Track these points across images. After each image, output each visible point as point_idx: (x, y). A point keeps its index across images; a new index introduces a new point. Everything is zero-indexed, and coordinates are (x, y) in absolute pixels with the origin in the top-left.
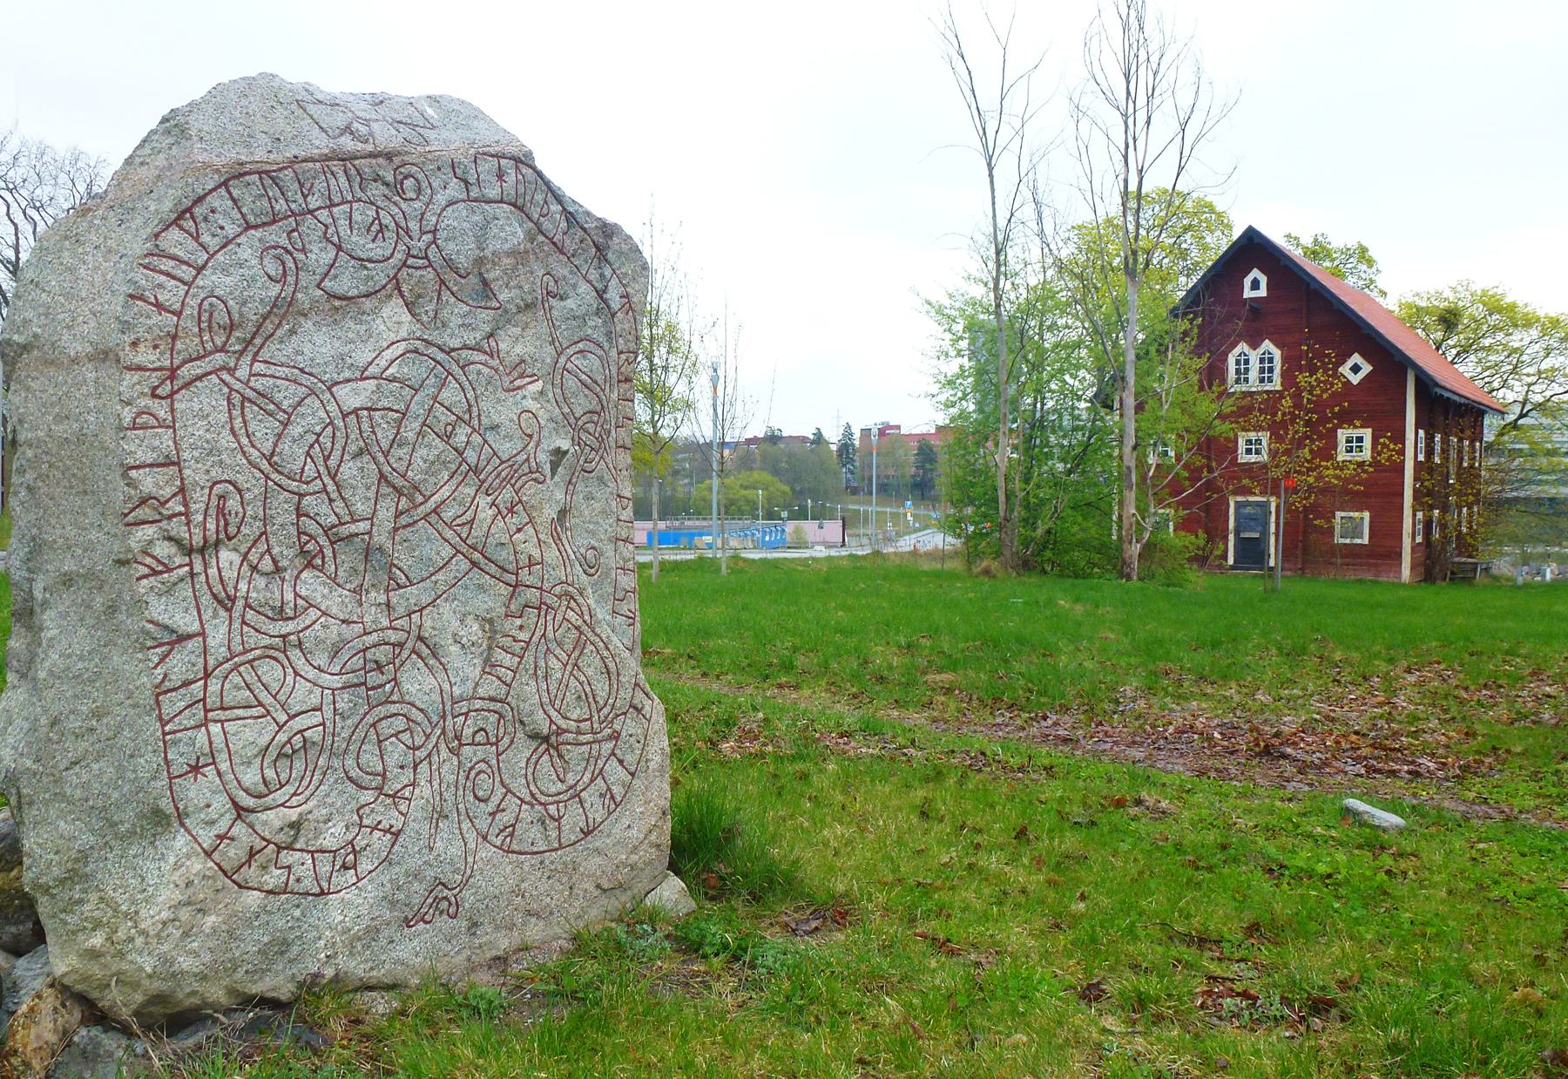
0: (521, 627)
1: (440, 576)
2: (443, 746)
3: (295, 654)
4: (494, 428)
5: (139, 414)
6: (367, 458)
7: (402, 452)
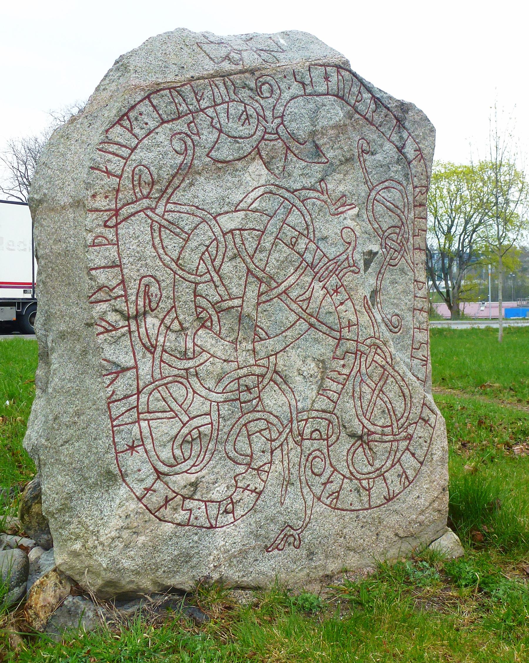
0: (344, 366)
1: (288, 333)
2: (290, 440)
3: (193, 380)
4: (324, 239)
5: (97, 237)
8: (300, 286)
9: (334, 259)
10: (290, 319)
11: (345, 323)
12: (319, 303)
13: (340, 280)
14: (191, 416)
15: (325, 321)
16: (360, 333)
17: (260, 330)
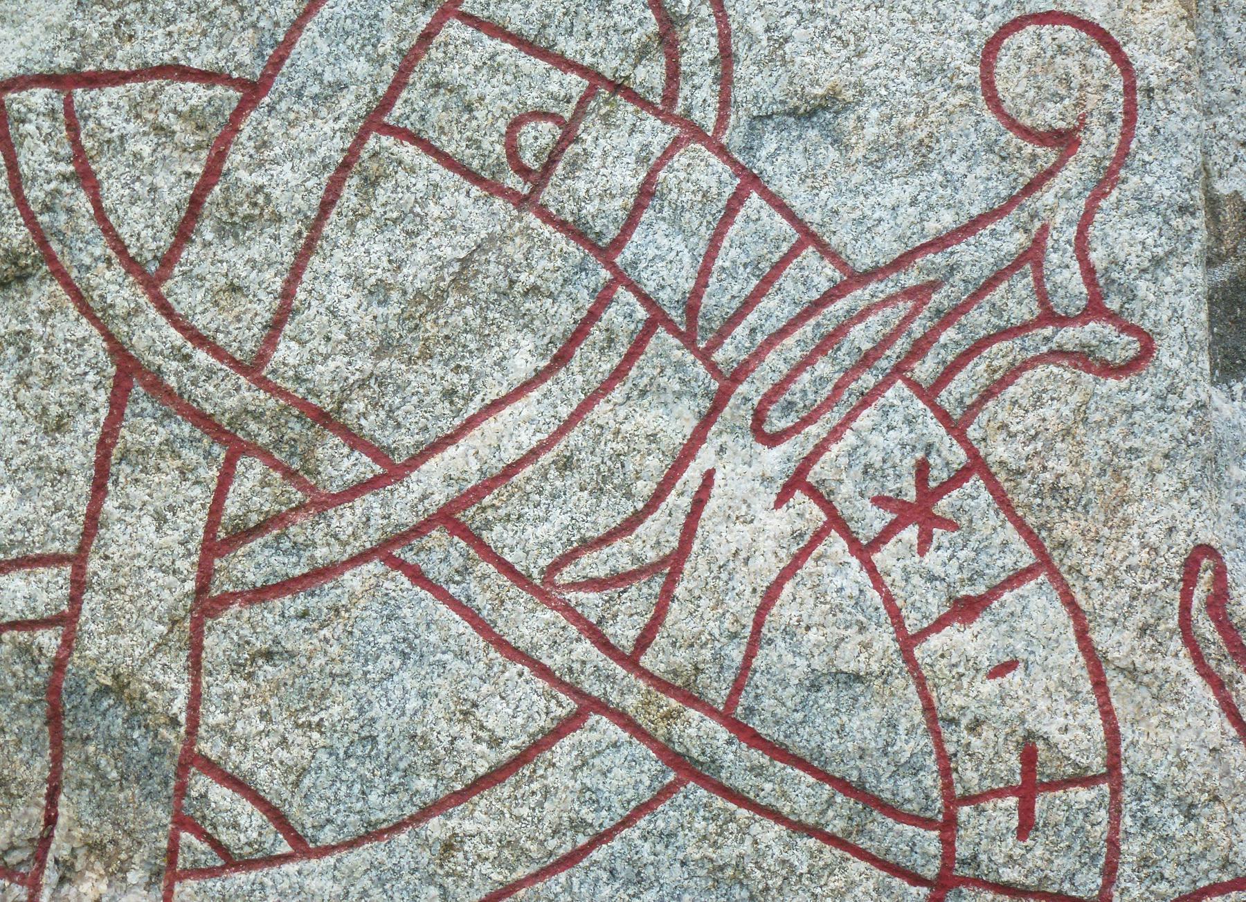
1: (476, 821)
4: (815, 112)
6: (44, 292)
7: (257, 260)
8: (586, 472)
9: (900, 264)
10: (496, 716)
11: (988, 758)
12: (743, 605)
13: (957, 429)
14: (1097, 764)
15: (802, 742)
16: (1132, 849)
17: (220, 795)
